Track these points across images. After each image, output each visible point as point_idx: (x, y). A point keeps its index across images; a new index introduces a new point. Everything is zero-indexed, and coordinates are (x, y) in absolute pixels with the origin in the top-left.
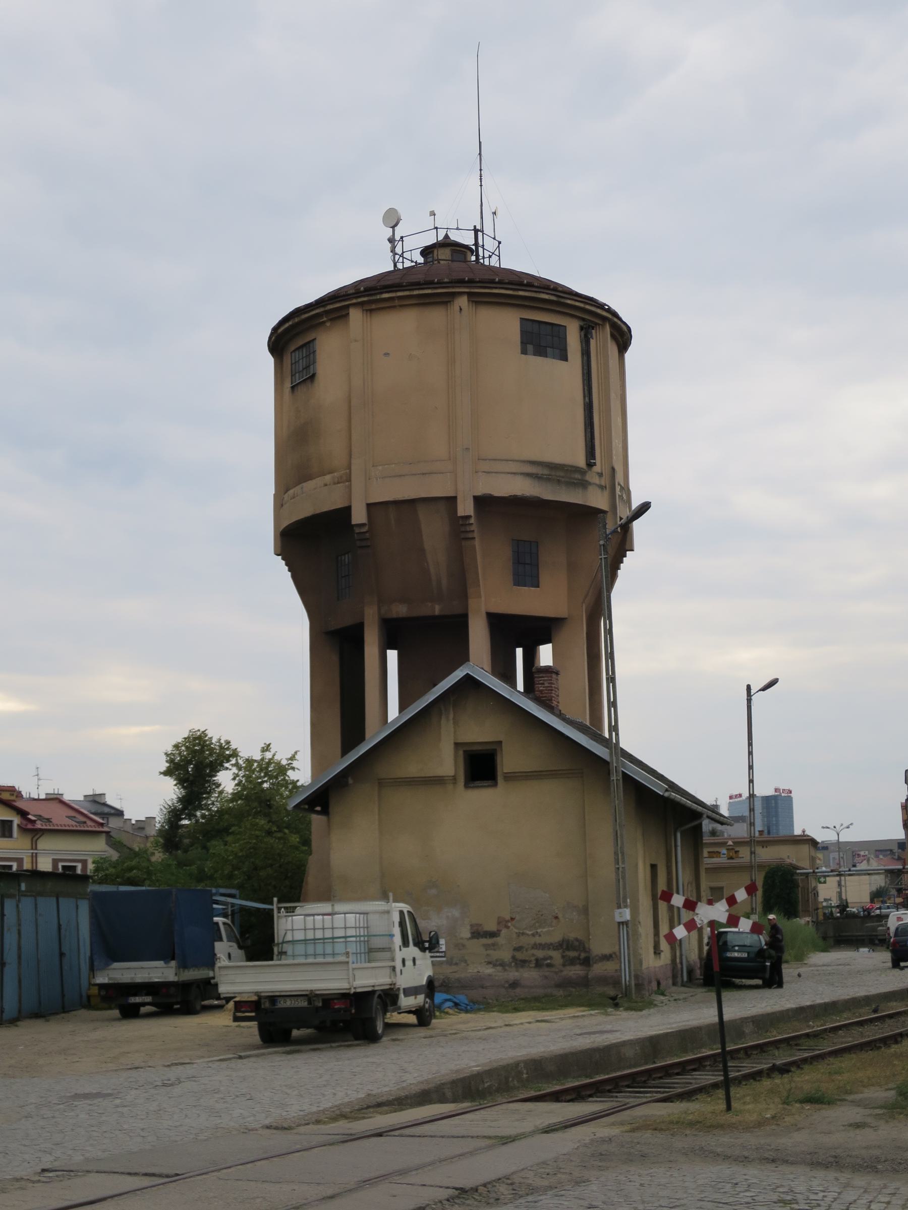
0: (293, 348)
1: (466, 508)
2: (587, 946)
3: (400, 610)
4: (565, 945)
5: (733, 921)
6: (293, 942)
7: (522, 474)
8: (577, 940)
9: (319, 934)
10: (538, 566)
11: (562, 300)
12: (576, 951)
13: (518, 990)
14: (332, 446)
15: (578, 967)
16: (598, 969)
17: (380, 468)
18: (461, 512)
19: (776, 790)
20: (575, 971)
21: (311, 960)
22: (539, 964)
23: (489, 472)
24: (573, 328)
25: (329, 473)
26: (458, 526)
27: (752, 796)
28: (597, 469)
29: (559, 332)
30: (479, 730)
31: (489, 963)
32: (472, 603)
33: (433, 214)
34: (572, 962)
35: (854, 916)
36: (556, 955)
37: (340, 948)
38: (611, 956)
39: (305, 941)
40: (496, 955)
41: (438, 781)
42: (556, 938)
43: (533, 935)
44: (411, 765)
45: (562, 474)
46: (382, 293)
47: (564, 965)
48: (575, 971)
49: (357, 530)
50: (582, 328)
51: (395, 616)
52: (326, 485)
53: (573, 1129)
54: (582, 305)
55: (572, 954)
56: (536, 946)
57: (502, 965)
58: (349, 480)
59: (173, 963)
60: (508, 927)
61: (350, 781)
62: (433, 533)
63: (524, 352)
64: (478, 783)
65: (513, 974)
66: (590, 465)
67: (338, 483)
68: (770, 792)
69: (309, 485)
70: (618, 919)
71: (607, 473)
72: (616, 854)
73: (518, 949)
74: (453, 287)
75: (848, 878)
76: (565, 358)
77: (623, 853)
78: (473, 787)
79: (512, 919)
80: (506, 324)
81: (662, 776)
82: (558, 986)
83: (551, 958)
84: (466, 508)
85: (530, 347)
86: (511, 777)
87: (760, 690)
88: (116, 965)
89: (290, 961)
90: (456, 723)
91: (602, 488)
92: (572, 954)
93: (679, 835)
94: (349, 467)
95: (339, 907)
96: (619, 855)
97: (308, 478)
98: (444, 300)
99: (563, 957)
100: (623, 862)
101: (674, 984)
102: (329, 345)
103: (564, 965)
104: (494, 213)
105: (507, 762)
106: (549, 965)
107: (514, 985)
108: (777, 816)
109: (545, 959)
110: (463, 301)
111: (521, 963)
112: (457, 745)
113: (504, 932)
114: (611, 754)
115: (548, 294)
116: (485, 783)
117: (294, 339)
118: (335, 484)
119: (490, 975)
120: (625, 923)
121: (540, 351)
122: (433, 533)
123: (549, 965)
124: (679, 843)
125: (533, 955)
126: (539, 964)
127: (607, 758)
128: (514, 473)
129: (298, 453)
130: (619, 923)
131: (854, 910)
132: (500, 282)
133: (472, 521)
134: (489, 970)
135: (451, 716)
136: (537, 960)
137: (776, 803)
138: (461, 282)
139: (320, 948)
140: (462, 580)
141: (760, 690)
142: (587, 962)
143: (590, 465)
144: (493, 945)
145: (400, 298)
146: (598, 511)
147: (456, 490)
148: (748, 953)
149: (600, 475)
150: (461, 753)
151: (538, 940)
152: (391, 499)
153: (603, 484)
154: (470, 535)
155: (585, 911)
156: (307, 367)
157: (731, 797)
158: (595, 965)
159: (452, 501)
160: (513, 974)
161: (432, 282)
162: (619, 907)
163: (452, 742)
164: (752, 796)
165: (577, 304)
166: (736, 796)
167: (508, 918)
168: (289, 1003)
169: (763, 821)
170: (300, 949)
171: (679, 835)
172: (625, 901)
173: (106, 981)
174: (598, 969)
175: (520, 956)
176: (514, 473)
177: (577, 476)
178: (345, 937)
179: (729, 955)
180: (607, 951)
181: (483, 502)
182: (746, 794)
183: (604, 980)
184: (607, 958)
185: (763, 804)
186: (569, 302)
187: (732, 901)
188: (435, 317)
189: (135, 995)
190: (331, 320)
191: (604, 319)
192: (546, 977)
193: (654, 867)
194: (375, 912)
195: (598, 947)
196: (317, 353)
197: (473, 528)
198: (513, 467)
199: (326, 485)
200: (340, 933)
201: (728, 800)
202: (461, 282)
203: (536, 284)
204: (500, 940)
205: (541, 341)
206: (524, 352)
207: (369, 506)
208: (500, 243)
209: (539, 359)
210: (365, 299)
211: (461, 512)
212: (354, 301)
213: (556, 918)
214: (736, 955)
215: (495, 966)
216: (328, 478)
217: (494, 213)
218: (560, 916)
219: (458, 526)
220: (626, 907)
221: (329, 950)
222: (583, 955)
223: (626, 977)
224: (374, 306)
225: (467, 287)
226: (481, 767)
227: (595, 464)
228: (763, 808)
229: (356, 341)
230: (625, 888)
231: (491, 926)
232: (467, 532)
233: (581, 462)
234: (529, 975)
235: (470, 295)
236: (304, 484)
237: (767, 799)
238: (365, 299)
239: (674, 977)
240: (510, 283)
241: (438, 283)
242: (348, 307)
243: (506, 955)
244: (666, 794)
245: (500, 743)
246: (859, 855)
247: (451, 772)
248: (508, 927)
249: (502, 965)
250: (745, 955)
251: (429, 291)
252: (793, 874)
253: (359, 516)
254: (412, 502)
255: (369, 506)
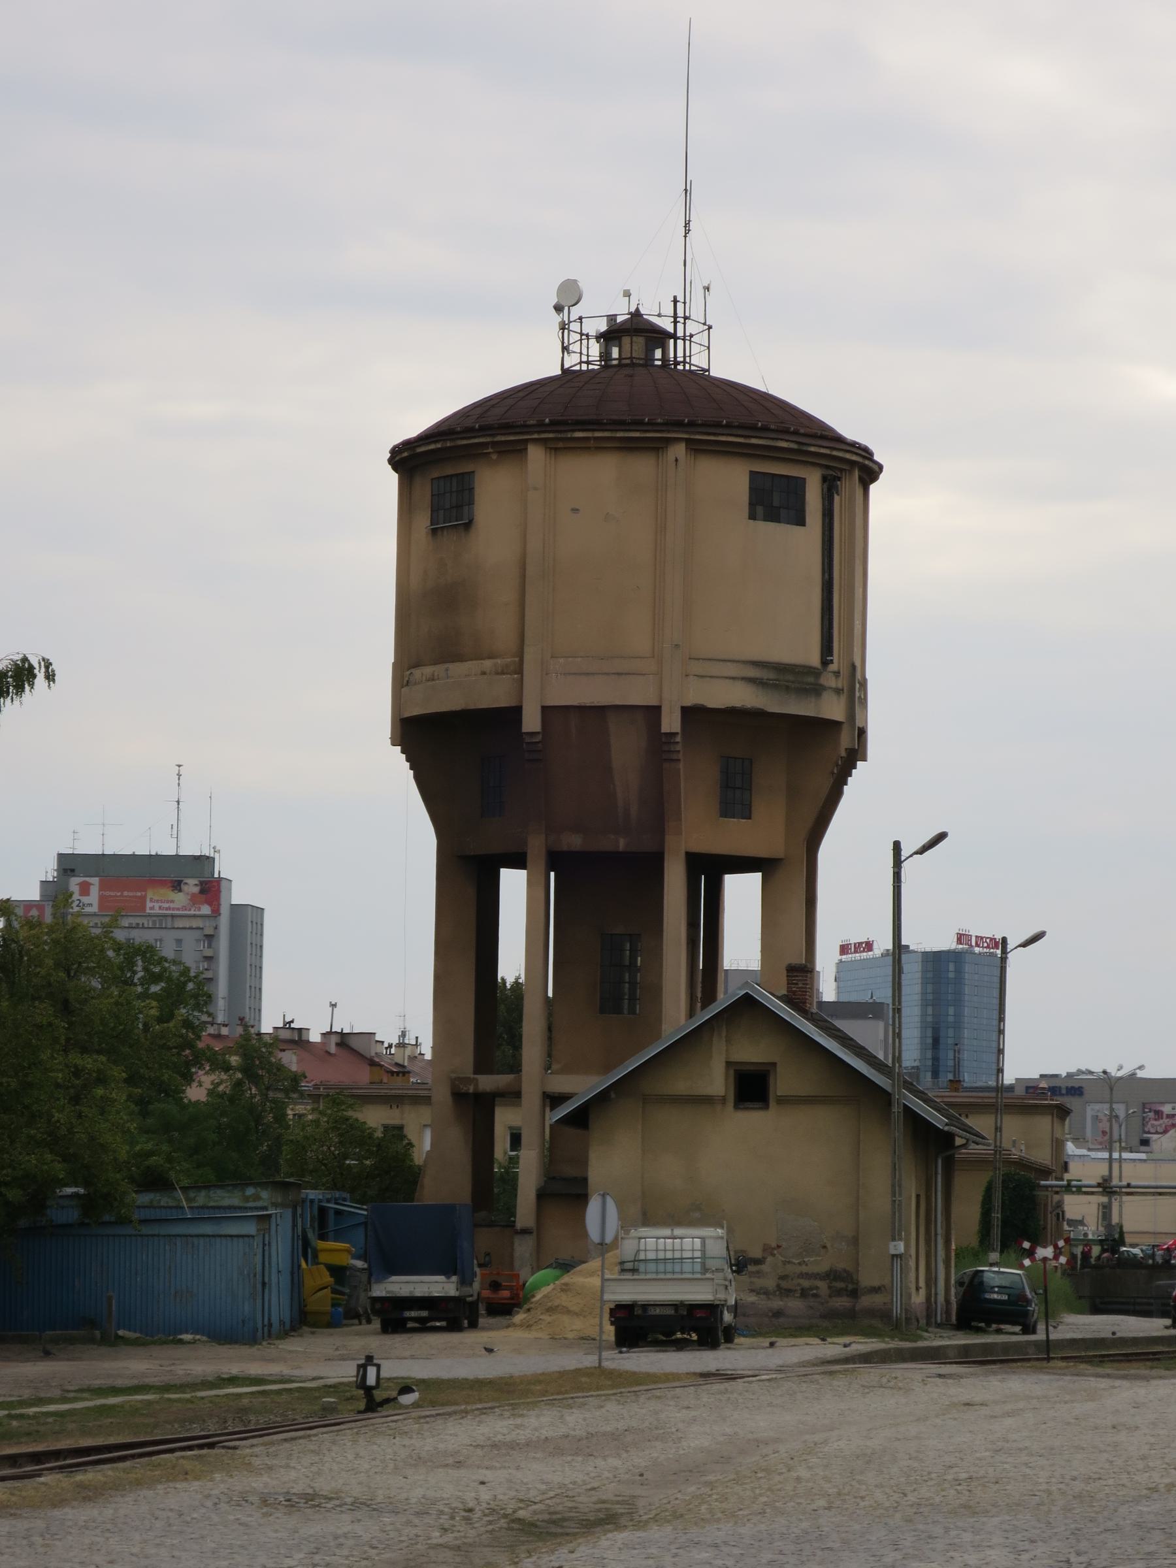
0: (436, 475)
1: (671, 723)
2: (855, 1277)
3: (573, 842)
4: (832, 1275)
5: (1056, 1257)
6: (645, 1261)
7: (743, 679)
8: (845, 1271)
9: (669, 1255)
10: (750, 790)
11: (805, 448)
12: (844, 1282)
13: (782, 1320)
14: (496, 621)
15: (845, 1299)
16: (866, 1301)
17: (562, 660)
18: (665, 728)
19: (961, 938)
20: (842, 1302)
21: (669, 1276)
22: (804, 1293)
23: (702, 677)
24: (808, 473)
25: (489, 658)
26: (659, 747)
27: (899, 949)
28: (833, 667)
29: (797, 487)
30: (752, 1050)
31: (752, 1291)
32: (670, 841)
33: (627, 294)
34: (839, 1293)
35: (1133, 1263)
36: (823, 1285)
37: (687, 1267)
38: (879, 1288)
39: (657, 1260)
40: (759, 1282)
41: (706, 1101)
42: (824, 1268)
43: (800, 1264)
44: (680, 1084)
45: (791, 678)
46: (574, 431)
47: (830, 1296)
48: (842, 1302)
49: (528, 740)
50: (824, 479)
51: (565, 848)
52: (484, 673)
53: (1145, 1230)
54: (827, 451)
55: (840, 1285)
56: (803, 1275)
57: (766, 1293)
58: (520, 671)
59: (454, 1278)
60: (774, 1255)
61: (613, 1095)
62: (626, 751)
63: (753, 516)
64: (748, 1104)
65: (777, 1303)
66: (825, 663)
67: (503, 673)
68: (947, 943)
69: (458, 669)
70: (893, 1252)
71: (845, 672)
72: (893, 1186)
73: (783, 1278)
74: (669, 432)
75: (1125, 1198)
76: (801, 521)
77: (900, 1186)
78: (747, 1109)
79: (779, 1247)
80: (730, 480)
81: (863, 1048)
82: (824, 1317)
83: (817, 1288)
84: (671, 723)
85: (760, 510)
86: (783, 1101)
87: (1020, 946)
88: (394, 1278)
89: (642, 1276)
90: (728, 1041)
91: (838, 691)
92: (840, 1285)
93: (940, 1162)
94: (520, 654)
95: (678, 1232)
96: (896, 1188)
97: (459, 658)
98: (657, 447)
99: (830, 1287)
100: (900, 1195)
101: (928, 1324)
102: (496, 490)
103: (830, 1296)
104: (707, 288)
105: (784, 1083)
106: (816, 1296)
107: (778, 1314)
108: (958, 1002)
109: (811, 1289)
110: (679, 450)
111: (785, 1292)
112: (729, 1064)
113: (769, 1259)
114: (893, 1085)
115: (787, 441)
116: (757, 1105)
117: (441, 468)
118: (497, 673)
119: (753, 1303)
120: (900, 1256)
121: (772, 515)
122: (626, 751)
123: (816, 1296)
124: (940, 1171)
125: (799, 1284)
126: (804, 1293)
127: (889, 1089)
128: (734, 678)
129: (432, 621)
130: (893, 1256)
131: (1136, 1251)
132: (728, 426)
133: (678, 739)
134: (752, 1298)
135: (724, 1034)
136: (802, 1289)
137: (959, 971)
138: (678, 424)
139: (669, 1267)
140: (659, 810)
141: (1020, 946)
142: (854, 1293)
143: (825, 663)
144: (758, 1272)
145: (596, 439)
146: (836, 724)
147: (661, 699)
148: (1009, 1295)
149: (837, 674)
150: (732, 1072)
151: (804, 1269)
152: (575, 703)
153: (840, 686)
154: (675, 757)
155: (855, 1241)
156: (459, 507)
157: (844, 949)
158: (863, 1298)
159: (653, 712)
160: (777, 1303)
161: (640, 423)
162: (894, 1239)
163: (724, 1060)
164: (899, 949)
165: (823, 451)
166: (858, 947)
167: (774, 1245)
168: (658, 1311)
169: (924, 1015)
170: (652, 1267)
171: (940, 1162)
172: (900, 1235)
173: (384, 1294)
174: (866, 1301)
175: (784, 1284)
176: (734, 678)
177: (811, 679)
178: (693, 1258)
179: (987, 1296)
180: (876, 1283)
181: (691, 714)
182: (884, 943)
183: (871, 1313)
184: (876, 1290)
185: (924, 971)
186: (812, 449)
187: (1056, 1247)
188: (642, 467)
189: (410, 1309)
190: (499, 452)
191: (853, 463)
192: (811, 1307)
193: (918, 1196)
194: (711, 1237)
195: (868, 1278)
196: (477, 491)
197: (679, 747)
198: (733, 670)
199: (484, 673)
200: (689, 1254)
201: (837, 956)
202: (678, 424)
203: (772, 427)
204: (765, 1268)
205: (774, 502)
206: (753, 516)
207: (544, 709)
208: (710, 327)
209: (771, 526)
210: (551, 435)
211: (665, 728)
212: (536, 436)
213: (825, 1247)
214: (995, 1296)
215: (758, 1293)
216: (488, 664)
217: (707, 288)
218: (828, 1245)
219: (659, 747)
220: (900, 1239)
221: (677, 1268)
222: (850, 1287)
223: (897, 1310)
224: (561, 445)
225: (687, 432)
226: (752, 1088)
227: (832, 662)
228: (925, 982)
229: (536, 489)
230: (900, 1220)
231: (756, 1253)
232: (669, 751)
233: (814, 660)
234: (794, 1305)
235: (687, 441)
236: (450, 666)
237: (935, 961)
238: (551, 435)
239: (928, 1317)
240: (742, 426)
241: (648, 424)
242: (527, 441)
243: (770, 1283)
244: (946, 1128)
245: (774, 1064)
246: (1159, 1114)
247: (722, 1093)
248: (774, 1255)
249: (766, 1293)
250: (1005, 1297)
251: (637, 435)
252: (1034, 1187)
253: (531, 722)
254: (601, 711)
255: (544, 709)
